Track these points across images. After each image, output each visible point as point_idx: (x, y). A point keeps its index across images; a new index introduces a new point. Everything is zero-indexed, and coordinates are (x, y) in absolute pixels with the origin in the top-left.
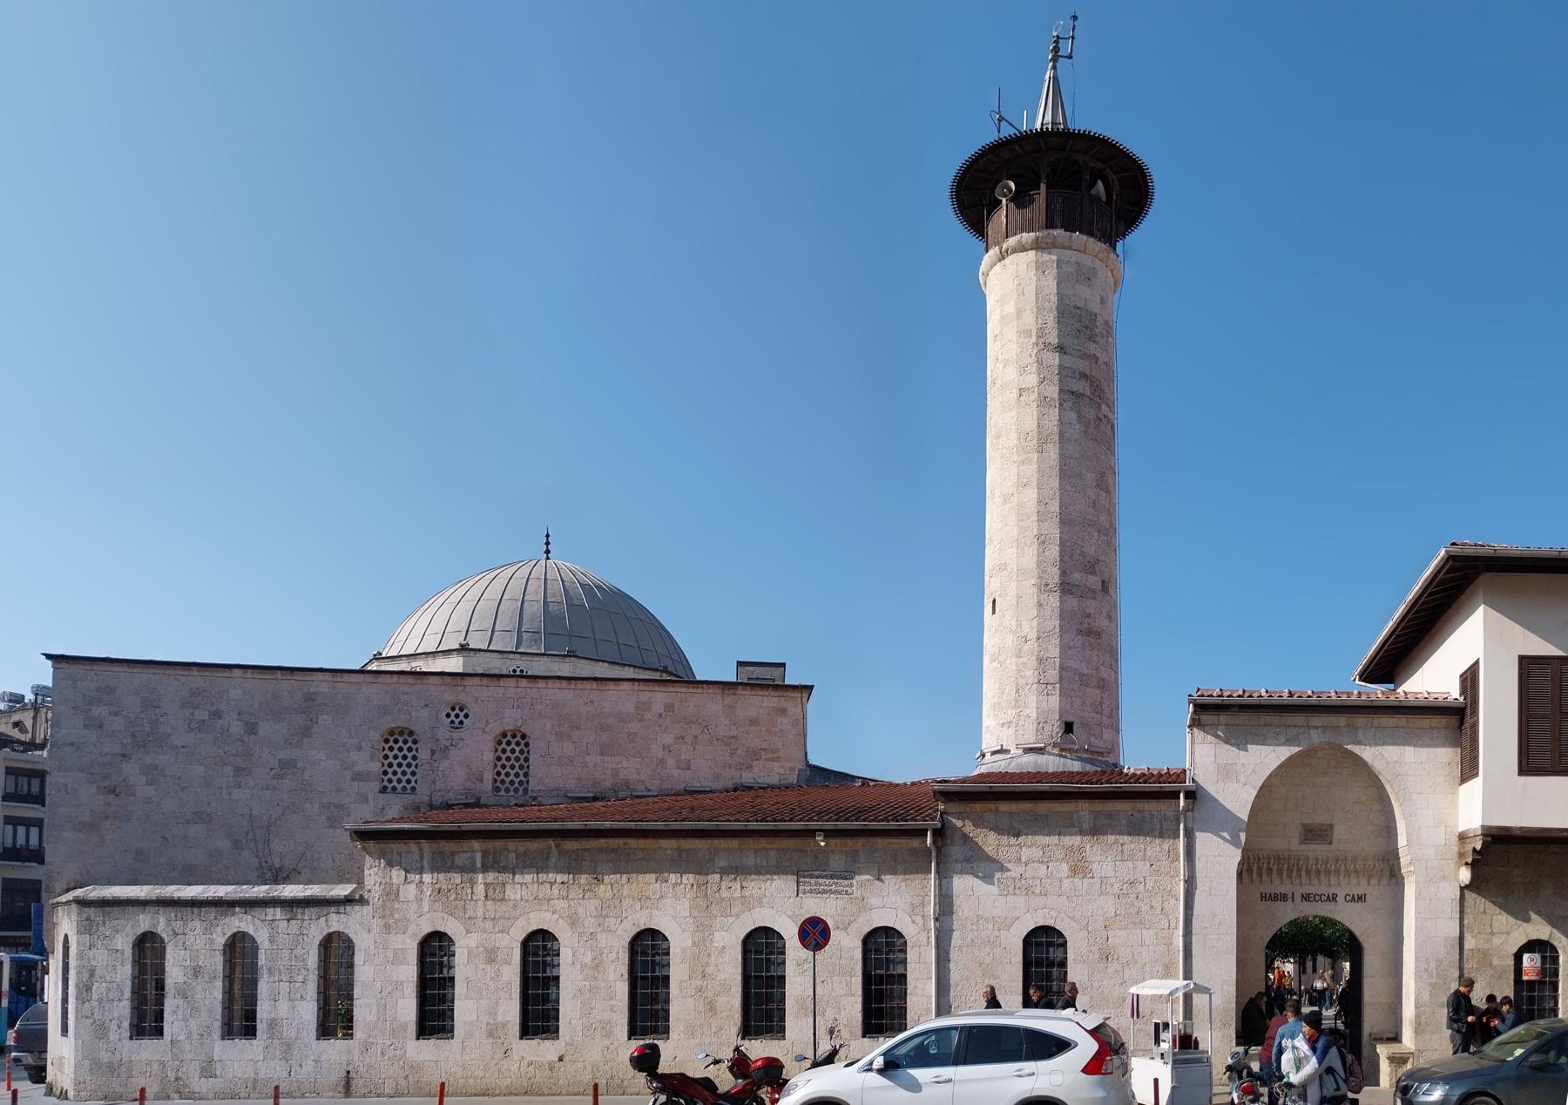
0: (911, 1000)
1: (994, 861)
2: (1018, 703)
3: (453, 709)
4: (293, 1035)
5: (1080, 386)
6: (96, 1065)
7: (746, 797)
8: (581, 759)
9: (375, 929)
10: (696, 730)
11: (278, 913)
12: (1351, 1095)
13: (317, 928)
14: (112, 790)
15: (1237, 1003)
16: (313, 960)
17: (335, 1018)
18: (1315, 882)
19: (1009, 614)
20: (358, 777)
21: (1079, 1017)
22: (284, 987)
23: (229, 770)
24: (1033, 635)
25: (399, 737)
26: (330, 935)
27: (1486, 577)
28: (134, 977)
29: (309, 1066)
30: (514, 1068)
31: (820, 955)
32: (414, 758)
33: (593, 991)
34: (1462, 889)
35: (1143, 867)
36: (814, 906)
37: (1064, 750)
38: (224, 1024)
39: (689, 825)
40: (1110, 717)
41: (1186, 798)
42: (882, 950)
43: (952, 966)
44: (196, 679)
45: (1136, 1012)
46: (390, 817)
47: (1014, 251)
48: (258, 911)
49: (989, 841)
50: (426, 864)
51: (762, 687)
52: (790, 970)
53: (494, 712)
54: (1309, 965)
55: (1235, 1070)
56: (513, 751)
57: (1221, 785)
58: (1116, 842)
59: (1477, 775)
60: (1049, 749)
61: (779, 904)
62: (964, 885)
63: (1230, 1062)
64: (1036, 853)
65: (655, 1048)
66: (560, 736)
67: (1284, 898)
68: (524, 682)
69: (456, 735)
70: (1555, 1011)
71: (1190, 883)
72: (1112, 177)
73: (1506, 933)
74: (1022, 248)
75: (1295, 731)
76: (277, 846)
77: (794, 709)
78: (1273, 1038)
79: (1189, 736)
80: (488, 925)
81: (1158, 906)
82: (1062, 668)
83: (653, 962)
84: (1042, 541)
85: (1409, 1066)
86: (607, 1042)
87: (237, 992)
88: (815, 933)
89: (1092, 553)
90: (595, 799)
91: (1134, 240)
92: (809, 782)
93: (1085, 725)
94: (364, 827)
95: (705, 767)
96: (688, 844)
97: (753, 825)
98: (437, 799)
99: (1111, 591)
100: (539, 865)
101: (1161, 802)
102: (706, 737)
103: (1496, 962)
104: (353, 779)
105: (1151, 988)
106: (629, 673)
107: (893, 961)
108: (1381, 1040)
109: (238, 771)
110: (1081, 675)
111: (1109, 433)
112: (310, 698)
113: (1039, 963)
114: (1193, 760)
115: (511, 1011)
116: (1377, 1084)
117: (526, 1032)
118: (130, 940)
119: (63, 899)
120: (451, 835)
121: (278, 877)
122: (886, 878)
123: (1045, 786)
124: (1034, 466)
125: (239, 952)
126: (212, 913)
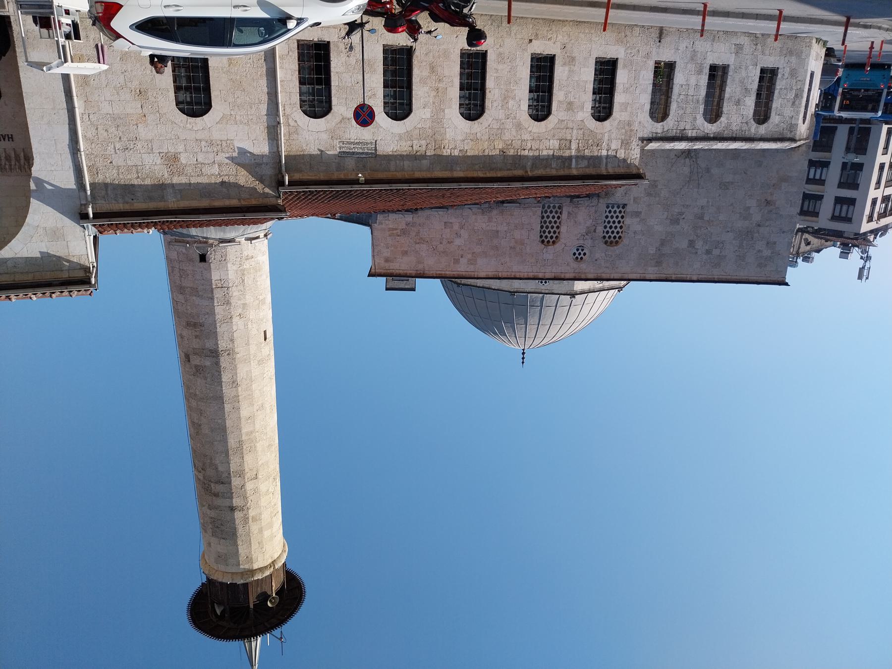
0: (295, 66)
1: (239, 164)
2: (242, 273)
3: (582, 258)
4: (689, 65)
5: (219, 488)
6: (799, 55)
7: (409, 205)
8: (512, 226)
9: (636, 124)
10: (441, 248)
11: (690, 134)
13: (670, 125)
14: (768, 203)
15: (15, 51)
16: (674, 107)
17: (664, 73)
19: (254, 332)
20: (637, 214)
22: (691, 92)
24: (235, 319)
25: (612, 240)
26: (662, 121)
28: (772, 101)
29: (682, 46)
30: (560, 37)
31: (360, 101)
32: (605, 227)
33: (508, 82)
35: (118, 160)
36: (365, 134)
37: (205, 242)
38: (727, 73)
42: (317, 102)
43: (266, 90)
46: (623, 188)
47: (266, 567)
48: (701, 134)
49: (244, 178)
50: (605, 161)
51: (399, 275)
52: (380, 91)
53: (558, 257)
56: (549, 232)
57: (59, 225)
60: (216, 243)
61: (388, 136)
62: (261, 147)
64: (207, 170)
65: (470, 44)
66: (522, 243)
68: (541, 275)
69: (581, 242)
76: (687, 170)
77: (380, 261)
80: (570, 125)
82: (212, 299)
83: (470, 100)
84: (234, 383)
86: (501, 50)
87: (718, 91)
88: (364, 116)
89: (199, 380)
90: (503, 202)
91: (196, 582)
92: (370, 215)
94: (637, 181)
95: (435, 224)
96: (446, 174)
97: (405, 187)
98: (595, 201)
99: (183, 355)
100: (538, 160)
101: (115, 209)
104: (640, 213)
106: (480, 283)
107: (309, 94)
109: (701, 217)
112: (658, 263)
115: (560, 73)
117: (551, 59)
118: (771, 120)
119: (802, 142)
120: (584, 179)
121: (687, 153)
123: (203, 218)
124: (244, 431)
125: (713, 112)
126: (726, 134)
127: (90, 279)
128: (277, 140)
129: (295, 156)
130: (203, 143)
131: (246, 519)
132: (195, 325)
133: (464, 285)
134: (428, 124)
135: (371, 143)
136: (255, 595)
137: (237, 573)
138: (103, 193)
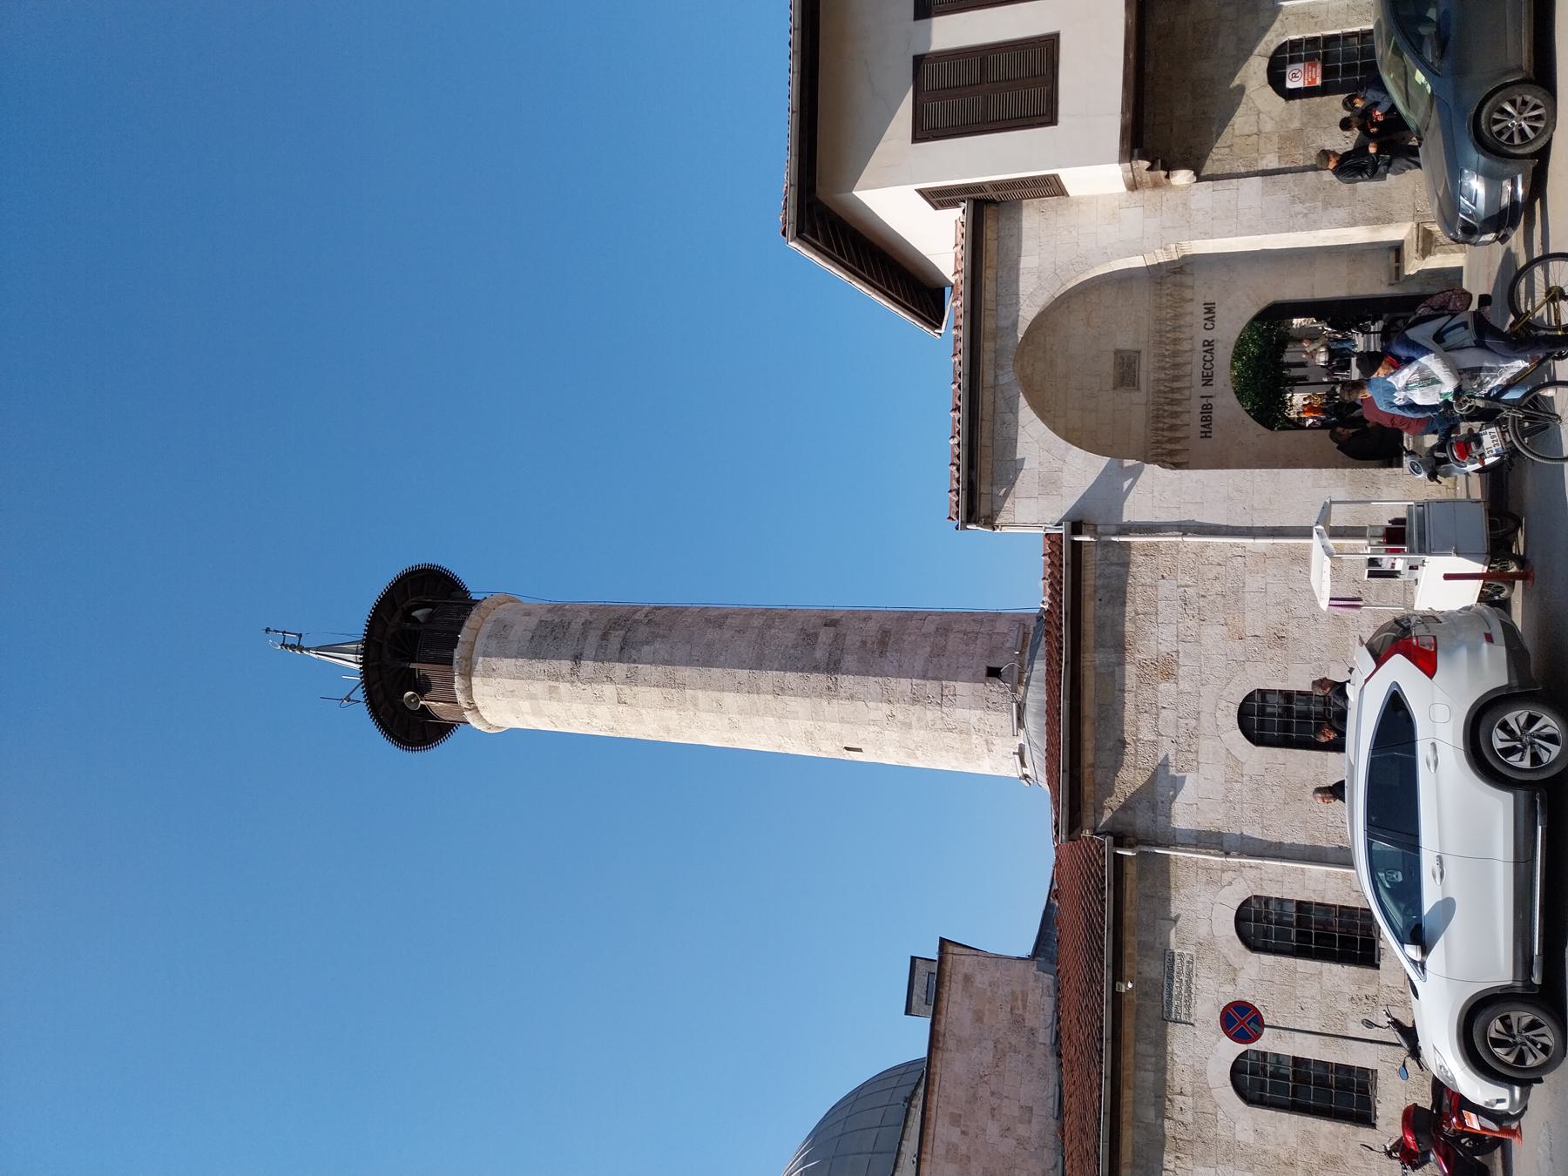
1: (1155, 774)
2: (964, 731)
10: (984, 1092)
12: (1474, 306)
15: (1344, 466)
18: (1188, 369)
19: (862, 733)
21: (1358, 677)
24: (886, 708)
27: (821, 192)
34: (1200, 178)
35: (1166, 588)
37: (1021, 680)
39: (1103, 1151)
40: (982, 623)
41: (1080, 533)
42: (1264, 927)
43: (1287, 840)
45: (1353, 602)
47: (471, 697)
49: (1130, 779)
54: (1296, 372)
55: (1435, 467)
57: (1064, 491)
58: (1133, 621)
59: (1056, 177)
60: (1018, 698)
61: (1201, 1056)
62: (1185, 815)
63: (1423, 475)
64: (1145, 722)
67: (1207, 409)
70: (1365, 36)
71: (1186, 528)
72: (410, 603)
73: (1258, 112)
74: (468, 689)
75: (1000, 402)
78: (1393, 417)
79: (1006, 530)
81: (1216, 570)
82: (924, 677)
85: (1436, 228)
89: (793, 636)
91: (474, 584)
92: (1054, 960)
93: (991, 653)
95: (1030, 1087)
97: (1106, 1068)
99: (837, 616)
101: (1085, 565)
102: (993, 1079)
103: (1296, 124)
105: (1322, 581)
107: (1280, 916)
108: (1399, 269)
110: (932, 655)
111: (664, 612)
113: (1286, 727)
114: (1034, 525)
116: (1460, 269)
122: (1174, 912)
123: (1064, 705)
124: (700, 694)
127: (975, 522)
128: (1196, 846)
129: (1168, 872)
130: (1193, 723)
131: (556, 677)
132: (883, 643)
133: (908, 1112)
134: (1224, 1134)
135: (1189, 1015)
136: (428, 674)
137: (472, 650)
138: (1114, 559)
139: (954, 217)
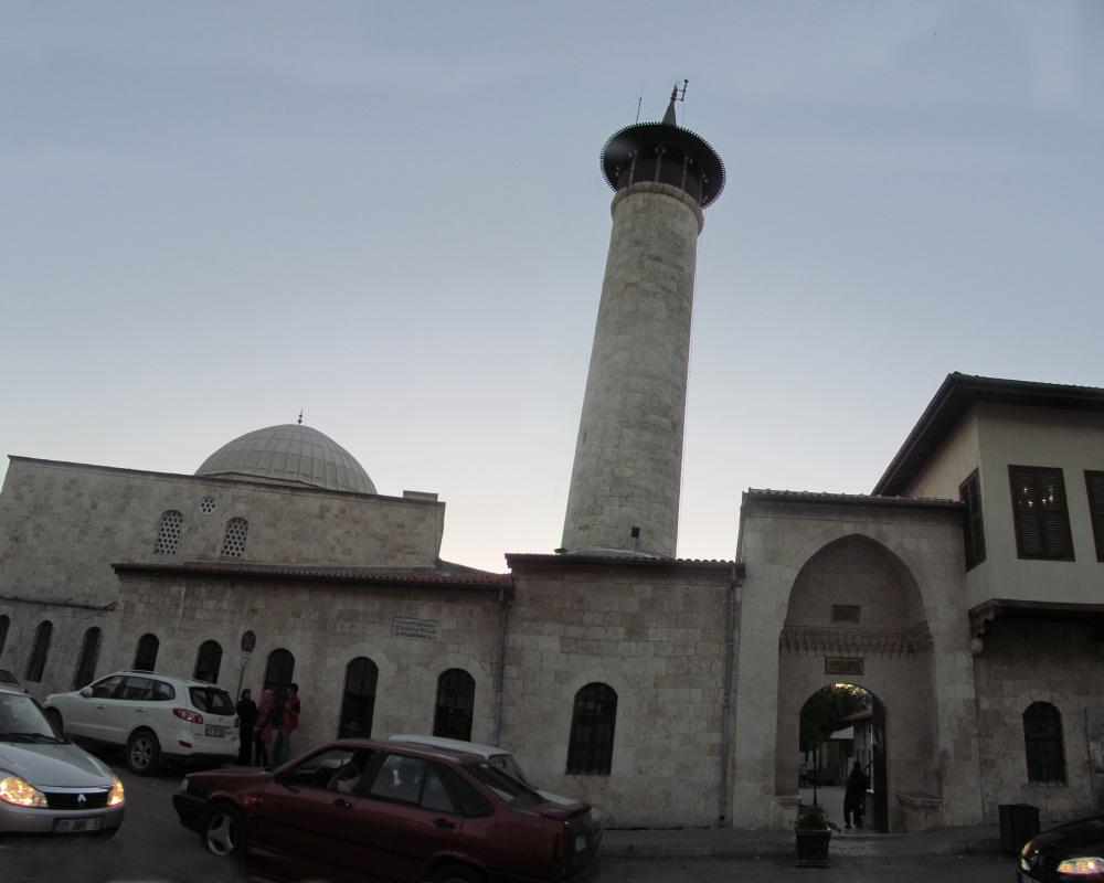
14: (16, 539)
23: (77, 530)
32: (179, 532)
44: (74, 474)
93: (649, 532)
103: (1008, 720)
104: (141, 543)
112: (129, 488)
135: (397, 634)
139: (954, 496)
